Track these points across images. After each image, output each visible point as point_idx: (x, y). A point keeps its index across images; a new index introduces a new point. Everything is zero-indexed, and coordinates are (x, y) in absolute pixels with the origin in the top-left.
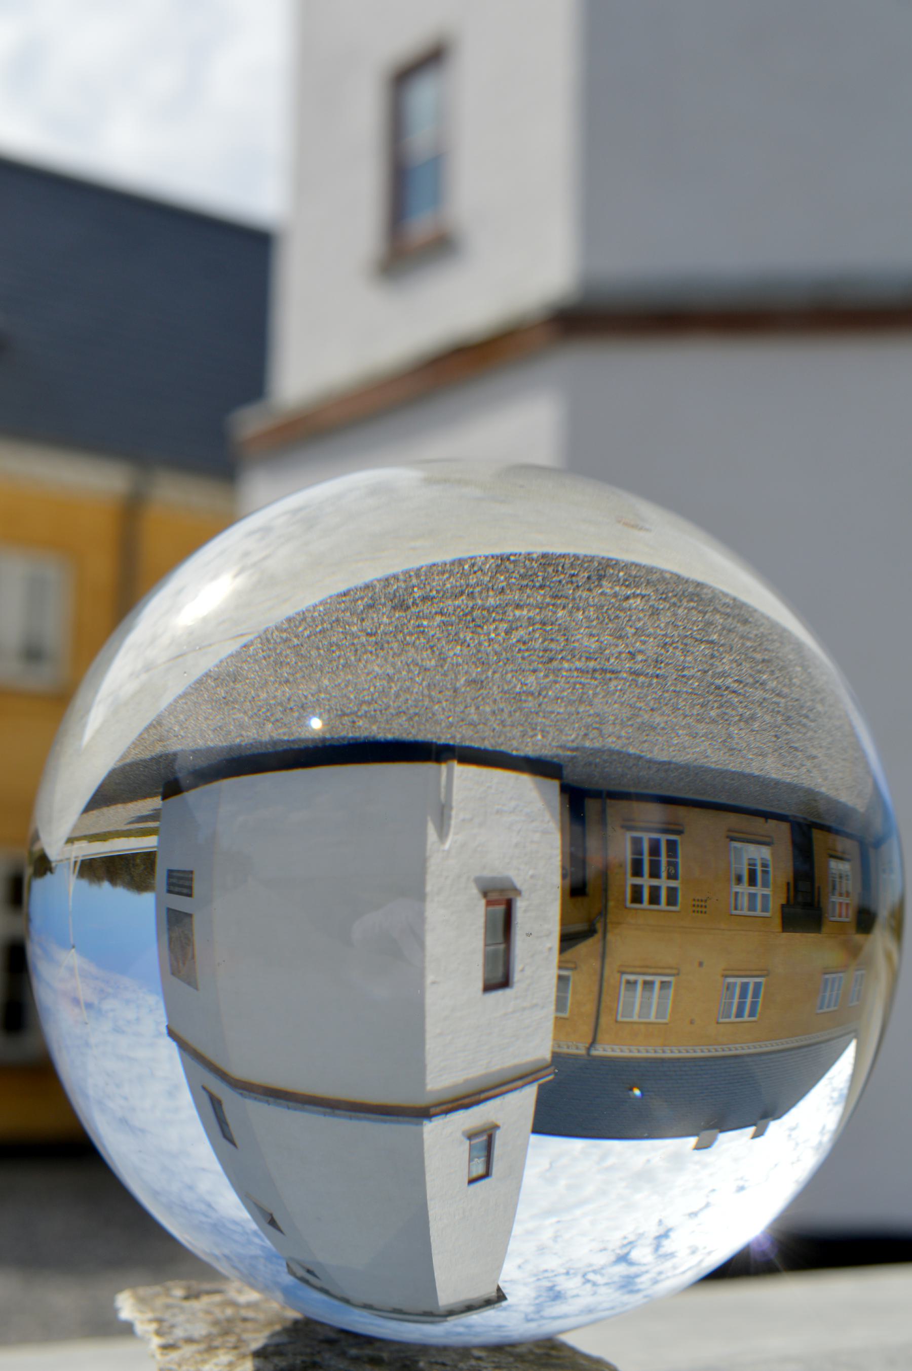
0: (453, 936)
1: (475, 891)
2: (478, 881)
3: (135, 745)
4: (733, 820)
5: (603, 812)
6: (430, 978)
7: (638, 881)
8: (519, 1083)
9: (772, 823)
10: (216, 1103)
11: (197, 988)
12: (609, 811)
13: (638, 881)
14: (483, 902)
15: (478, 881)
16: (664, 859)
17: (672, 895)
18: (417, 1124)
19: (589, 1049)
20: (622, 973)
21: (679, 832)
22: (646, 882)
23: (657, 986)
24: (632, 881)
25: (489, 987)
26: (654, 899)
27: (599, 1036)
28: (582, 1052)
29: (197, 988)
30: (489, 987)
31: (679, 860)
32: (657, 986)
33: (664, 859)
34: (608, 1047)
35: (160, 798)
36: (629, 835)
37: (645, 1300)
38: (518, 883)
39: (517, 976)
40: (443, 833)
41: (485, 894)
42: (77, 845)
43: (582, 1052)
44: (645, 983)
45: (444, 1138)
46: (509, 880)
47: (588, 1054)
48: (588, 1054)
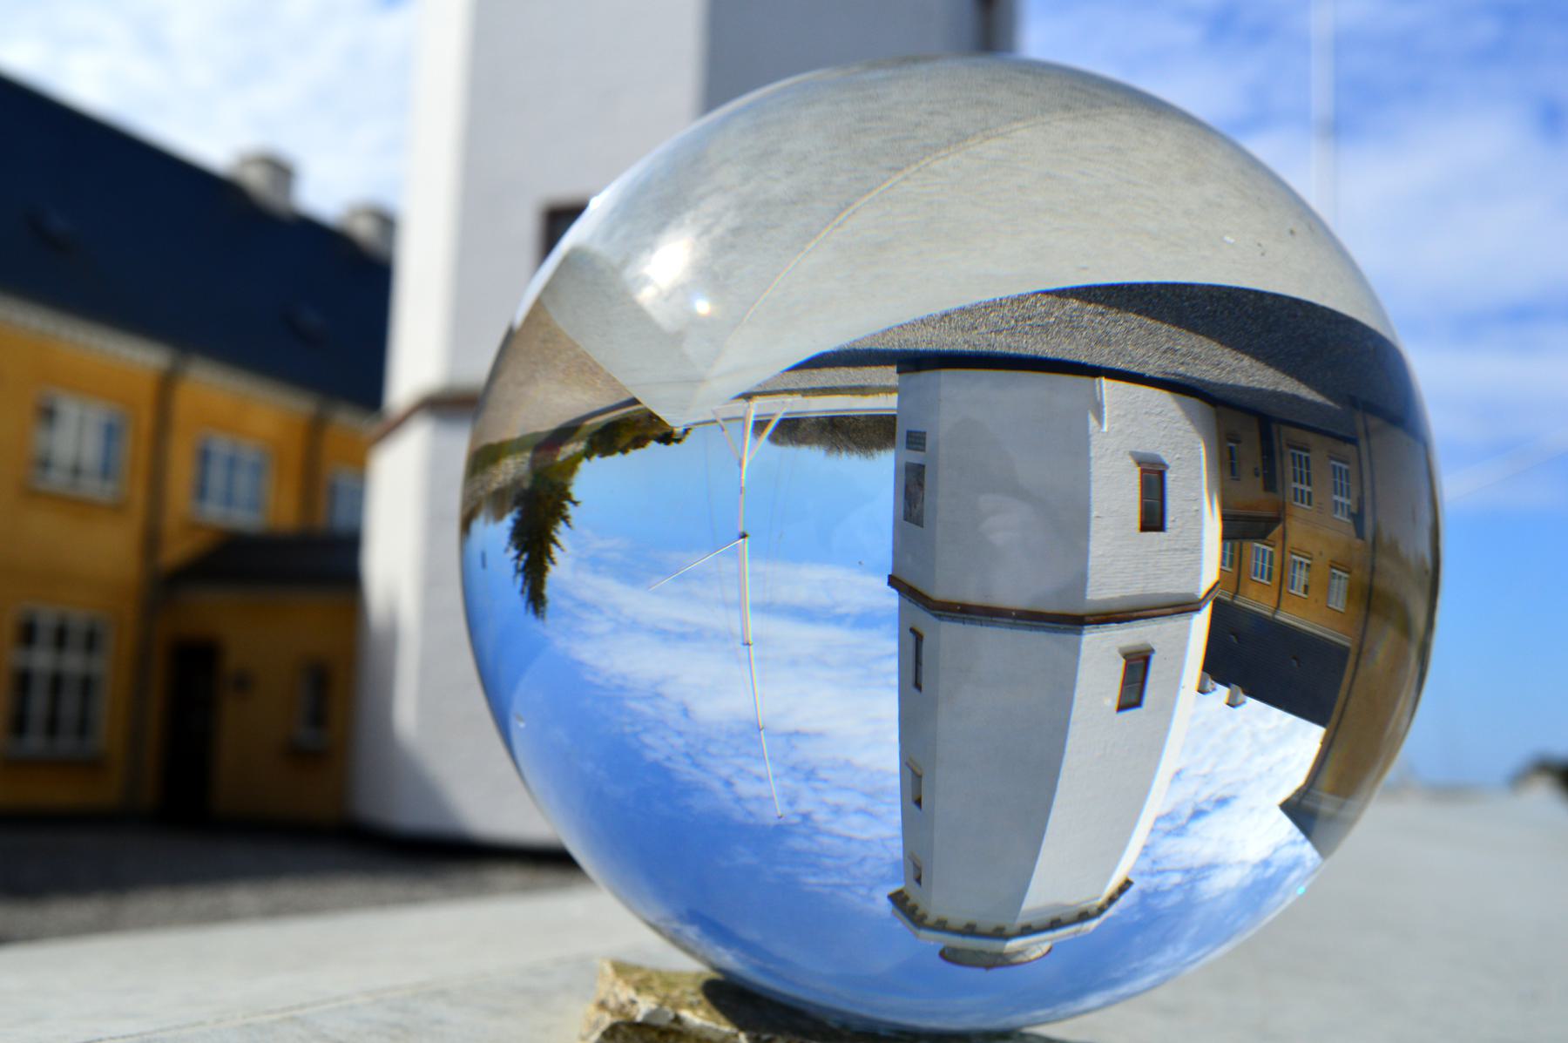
0: (1114, 495)
1: (1131, 461)
2: (1133, 454)
6: (1094, 514)
10: (918, 638)
14: (1138, 469)
15: (1133, 454)
17: (27, 634)
18: (1070, 637)
21: (1307, 451)
38: (1167, 461)
39: (1168, 524)
41: (1139, 463)
42: (758, 401)
45: (1101, 652)
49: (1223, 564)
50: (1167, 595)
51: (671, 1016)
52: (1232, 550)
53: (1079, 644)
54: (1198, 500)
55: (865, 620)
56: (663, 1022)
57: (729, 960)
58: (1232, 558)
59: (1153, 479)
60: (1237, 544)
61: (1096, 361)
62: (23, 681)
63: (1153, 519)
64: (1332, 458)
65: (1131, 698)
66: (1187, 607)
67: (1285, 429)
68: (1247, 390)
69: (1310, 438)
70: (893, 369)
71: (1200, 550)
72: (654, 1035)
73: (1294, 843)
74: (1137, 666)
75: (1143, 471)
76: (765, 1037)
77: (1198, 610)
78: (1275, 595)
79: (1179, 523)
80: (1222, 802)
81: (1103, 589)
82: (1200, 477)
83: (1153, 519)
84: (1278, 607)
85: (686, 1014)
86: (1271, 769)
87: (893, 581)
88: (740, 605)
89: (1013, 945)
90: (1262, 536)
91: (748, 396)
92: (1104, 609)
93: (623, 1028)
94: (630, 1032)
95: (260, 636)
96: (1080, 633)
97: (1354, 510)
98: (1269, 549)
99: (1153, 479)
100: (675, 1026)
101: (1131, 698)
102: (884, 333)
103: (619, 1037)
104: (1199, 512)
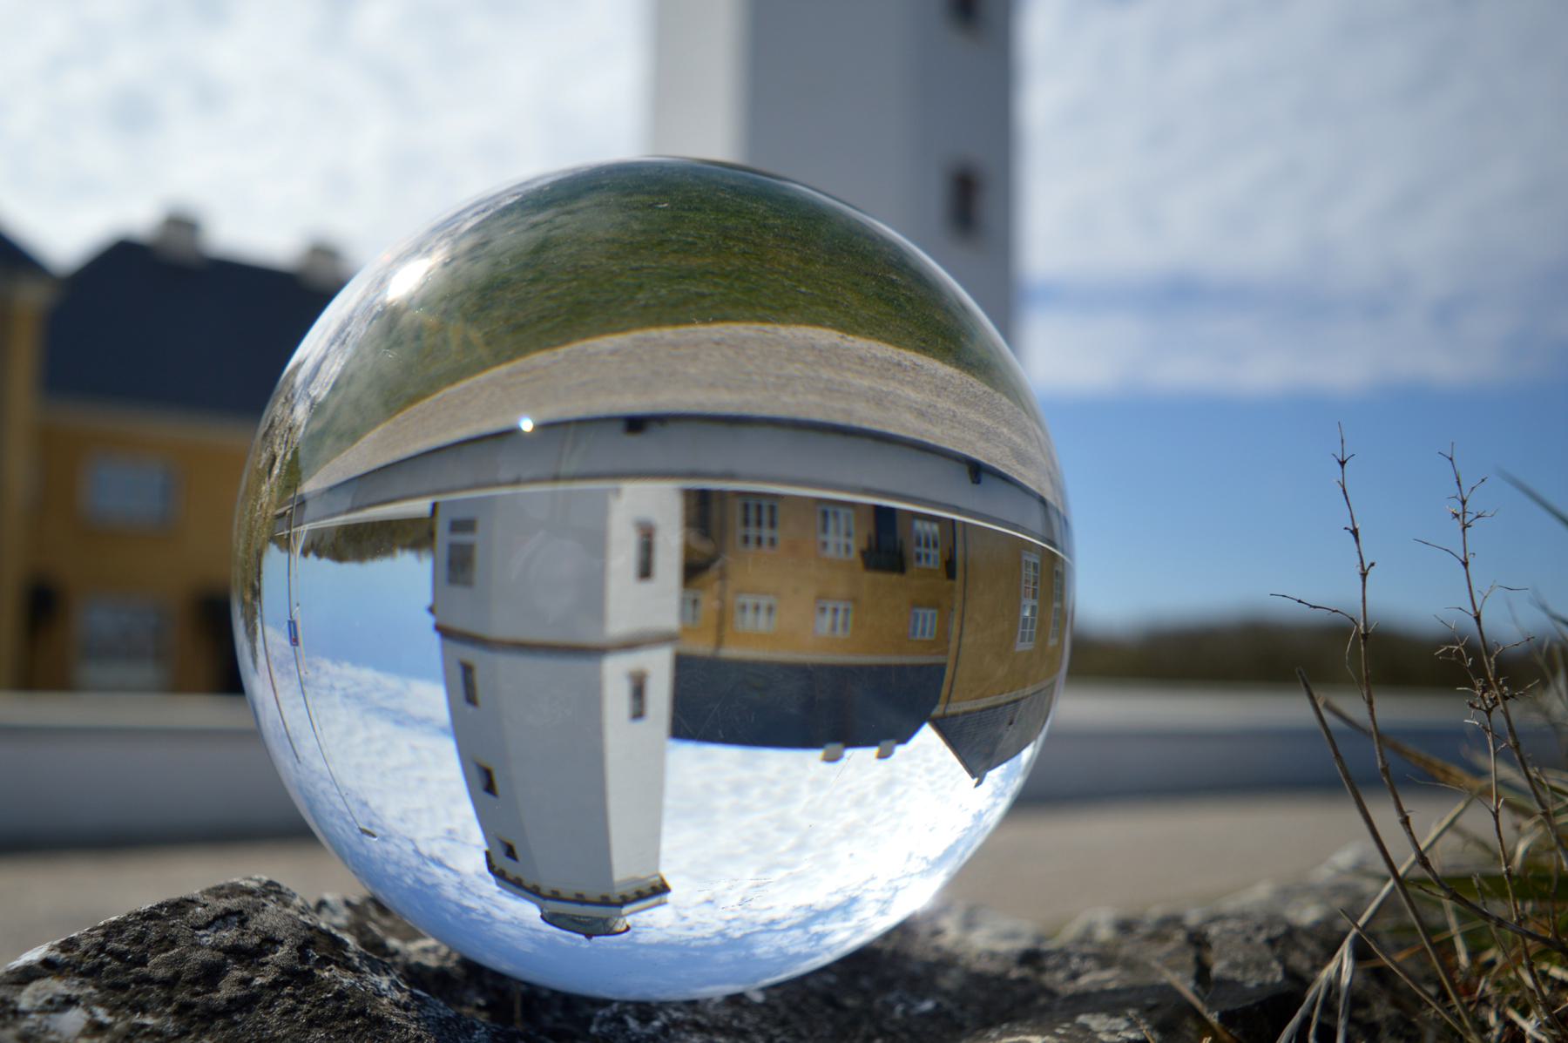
0: (622, 556)
17: (772, 542)
62: (772, 524)
81: (618, 624)
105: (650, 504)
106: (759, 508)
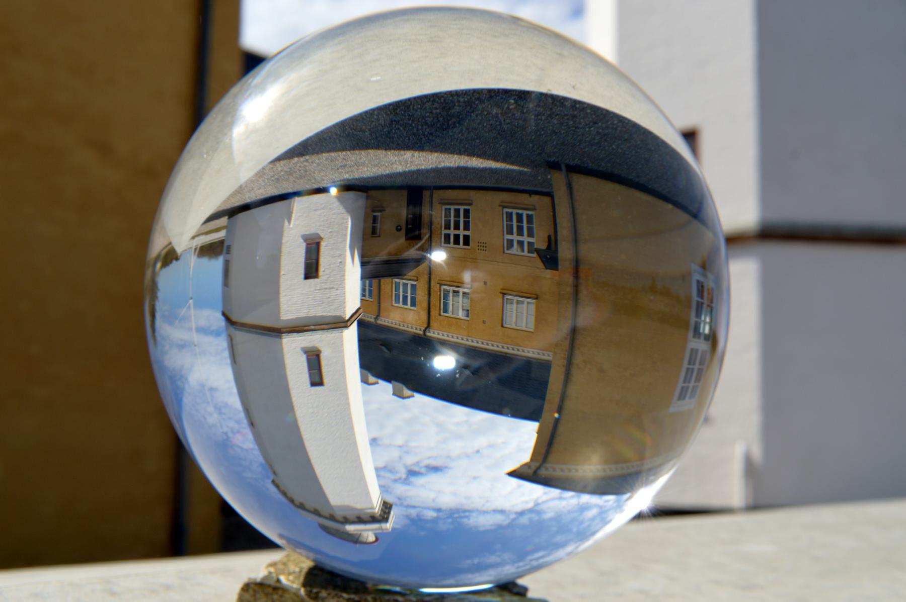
0: (293, 258)
1: (302, 240)
3: (224, 201)
4: (505, 196)
5: (431, 196)
6: (282, 272)
7: (447, 232)
8: (325, 327)
9: (535, 199)
11: (513, 474)
12: (434, 196)
13: (447, 232)
16: (462, 220)
18: (277, 340)
19: (424, 331)
20: (441, 285)
21: (470, 204)
22: (452, 232)
23: (461, 294)
24: (444, 232)
25: (307, 277)
26: (457, 241)
27: (432, 324)
28: (421, 333)
29: (513, 474)
30: (307, 277)
31: (505, 223)
32: (461, 294)
33: (462, 220)
34: (436, 332)
35: (226, 218)
36: (444, 207)
37: (157, 246)
38: (322, 236)
39: (321, 273)
40: (289, 222)
41: (305, 240)
42: (197, 239)
43: (421, 333)
44: (454, 292)
45: (293, 348)
46: (318, 234)
47: (425, 334)
48: (425, 334)
49: (363, 295)
50: (322, 317)
51: (275, 579)
52: (370, 285)
53: (281, 344)
54: (342, 256)
55: (217, 334)
56: (272, 582)
57: (319, 557)
58: (370, 291)
59: (313, 248)
60: (375, 281)
61: (290, 190)
62: (467, 227)
63: (311, 270)
64: (504, 207)
65: (317, 380)
66: (340, 324)
67: (438, 195)
68: (388, 176)
69: (472, 194)
70: (226, 218)
71: (349, 285)
72: (270, 590)
73: (238, 422)
74: (314, 359)
75: (307, 244)
76: (315, 590)
77: (347, 327)
78: (375, 308)
79: (327, 272)
80: (436, 469)
82: (345, 240)
83: (311, 270)
84: (429, 325)
85: (283, 578)
86: (478, 451)
87: (224, 314)
88: (190, 329)
89: (350, 528)
90: (398, 275)
91: (193, 238)
92: (291, 325)
93: (252, 586)
94: (257, 588)
95: (392, 245)
96: (281, 338)
97: (543, 246)
98: (410, 283)
99: (313, 248)
100: (278, 585)
101: (317, 380)
102: (228, 198)
103: (251, 591)
104: (342, 263)
105: (326, 216)
106: (457, 212)
